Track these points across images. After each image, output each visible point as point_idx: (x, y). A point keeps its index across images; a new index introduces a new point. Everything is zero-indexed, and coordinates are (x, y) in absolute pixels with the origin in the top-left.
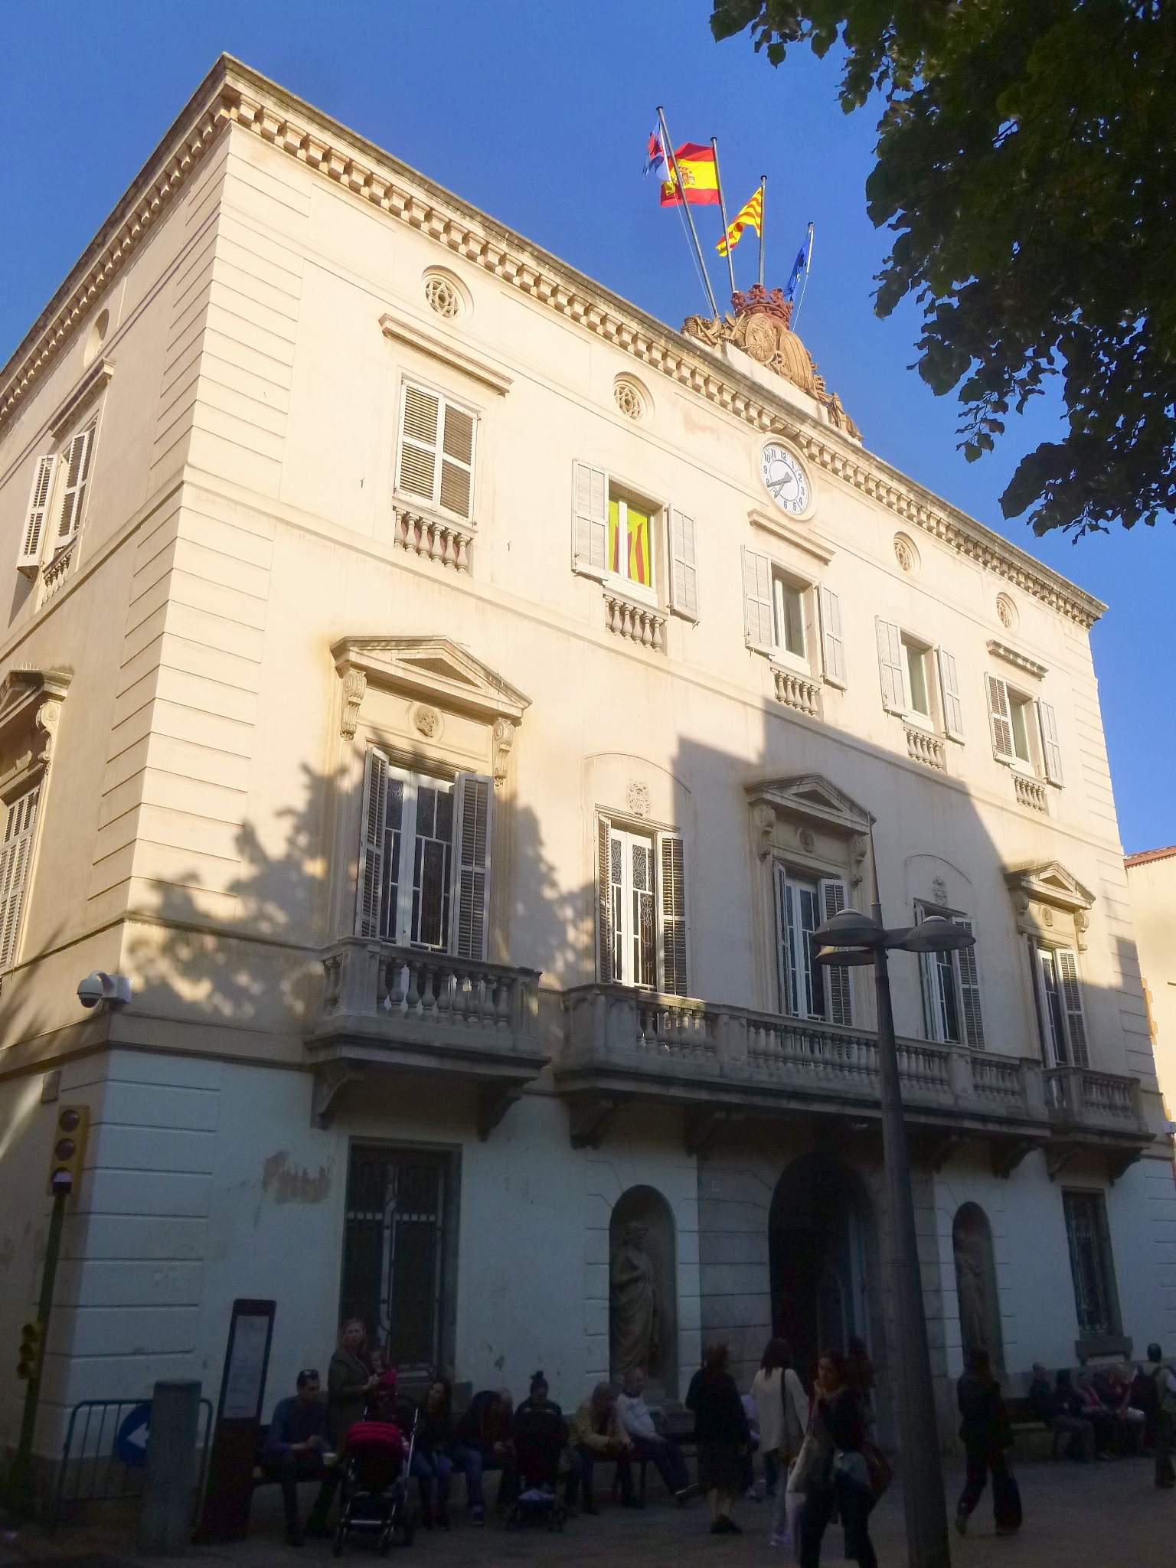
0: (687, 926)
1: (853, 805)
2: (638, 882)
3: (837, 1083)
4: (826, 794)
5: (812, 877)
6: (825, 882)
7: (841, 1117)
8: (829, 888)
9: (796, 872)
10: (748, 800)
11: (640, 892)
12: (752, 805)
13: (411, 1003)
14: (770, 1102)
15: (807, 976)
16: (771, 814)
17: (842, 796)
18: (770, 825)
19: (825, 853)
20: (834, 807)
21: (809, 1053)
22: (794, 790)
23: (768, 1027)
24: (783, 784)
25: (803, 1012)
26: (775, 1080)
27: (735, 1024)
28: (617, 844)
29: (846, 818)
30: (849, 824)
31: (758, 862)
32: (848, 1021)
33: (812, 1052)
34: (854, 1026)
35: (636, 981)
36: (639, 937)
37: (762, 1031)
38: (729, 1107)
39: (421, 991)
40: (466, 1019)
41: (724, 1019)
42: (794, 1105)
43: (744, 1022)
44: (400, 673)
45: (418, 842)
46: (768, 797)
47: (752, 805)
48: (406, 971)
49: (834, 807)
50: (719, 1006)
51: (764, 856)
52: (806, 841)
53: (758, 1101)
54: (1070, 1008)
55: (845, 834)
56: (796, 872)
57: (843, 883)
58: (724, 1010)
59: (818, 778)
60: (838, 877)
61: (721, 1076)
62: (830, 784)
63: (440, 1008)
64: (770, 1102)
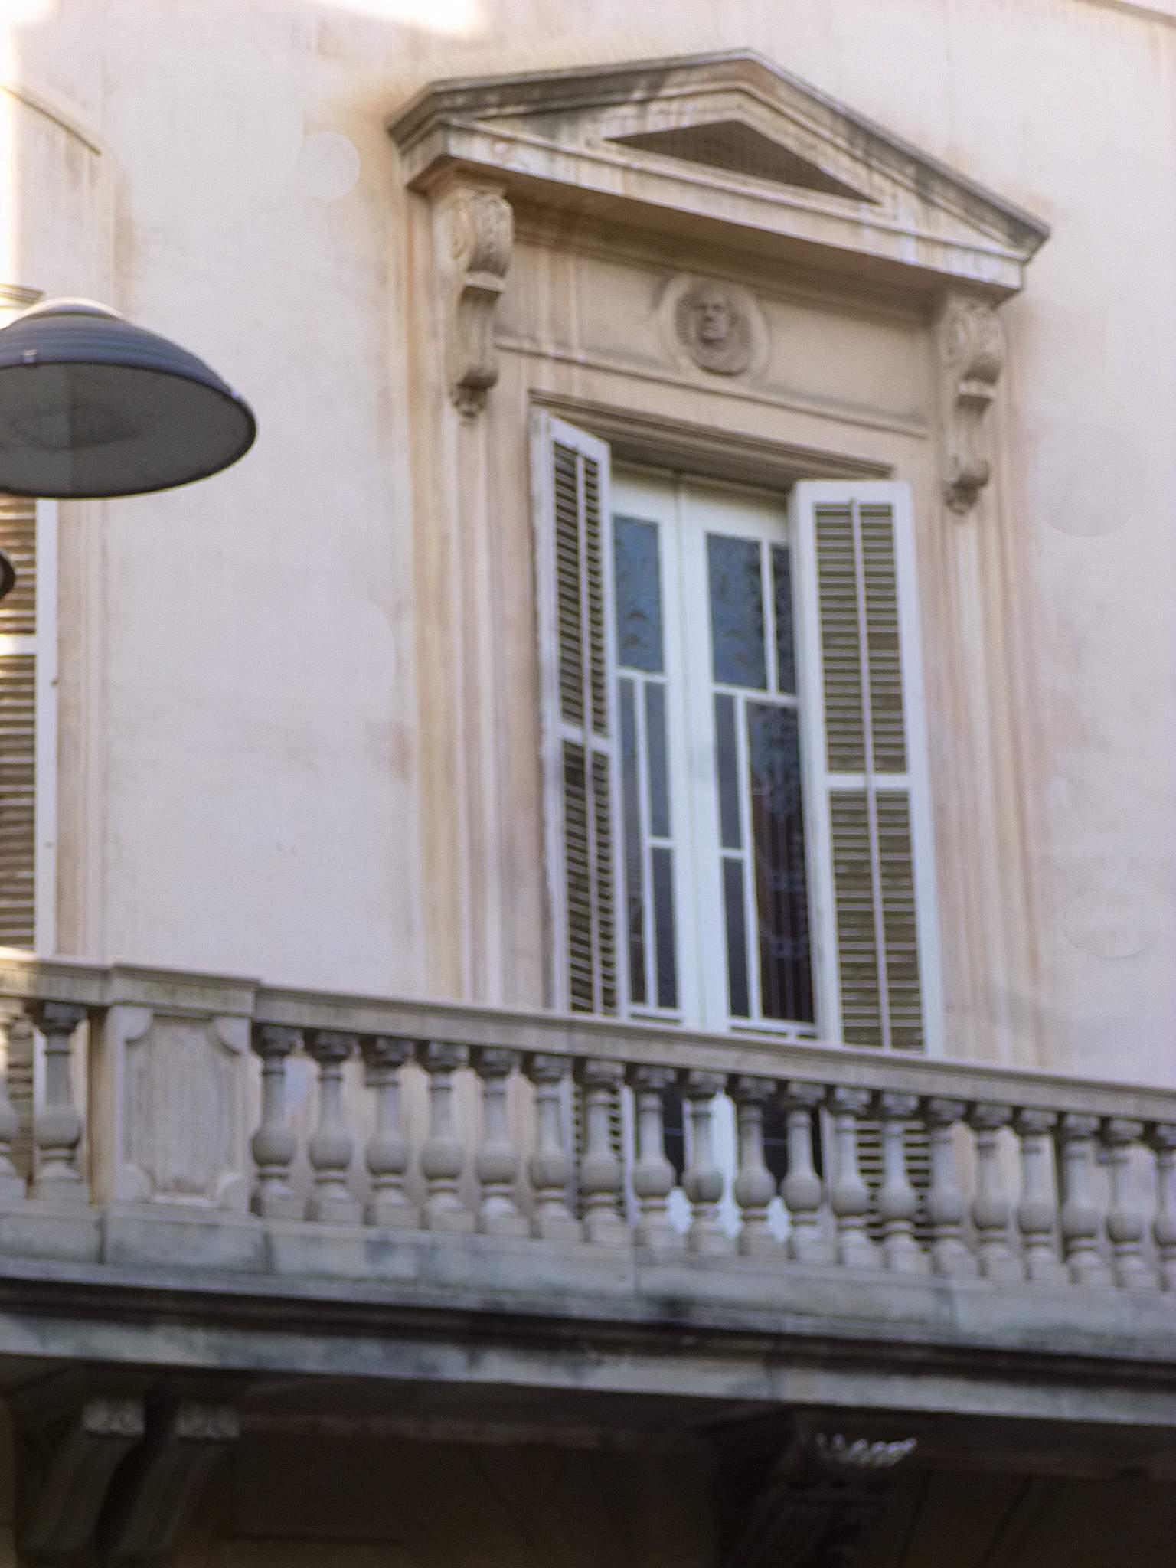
0: (45, 673)
1: (928, 177)
2: (736, 658)
3: (890, 1286)
4: (787, 136)
5: (759, 477)
6: (810, 494)
7: (783, 1416)
8: (830, 518)
9: (656, 456)
10: (404, 172)
11: (773, 696)
12: (424, 190)
13: (750, 1205)
14: (368, 1358)
15: (732, 872)
16: (495, 218)
17: (870, 140)
18: (485, 261)
19: (806, 377)
20: (855, 196)
21: (655, 1160)
22: (622, 120)
23: (432, 1058)
24: (557, 98)
25: (703, 999)
26: (401, 1265)
27: (188, 1048)
28: (639, 542)
29: (895, 228)
30: (909, 253)
31: (451, 418)
32: (909, 1036)
33: (582, 1140)
34: (935, 1049)
35: (739, 1006)
36: (746, 854)
37: (352, 1070)
38: (160, 1390)
39: (778, 1162)
40: (580, 1211)
41: (125, 1023)
42: (502, 1368)
43: (238, 1033)
44: (610, 183)
45: (724, 708)
46: (477, 151)
47: (424, 190)
48: (722, 1108)
49: (855, 196)
50: (104, 974)
51: (474, 390)
52: (710, 342)
53: (312, 1355)
54: (843, 758)
55: (910, 299)
56: (656, 456)
57: (905, 498)
58: (120, 988)
59: (742, 72)
60: (882, 472)
61: (100, 1259)
62: (808, 95)
63: (792, 1208)
64: (368, 1358)
